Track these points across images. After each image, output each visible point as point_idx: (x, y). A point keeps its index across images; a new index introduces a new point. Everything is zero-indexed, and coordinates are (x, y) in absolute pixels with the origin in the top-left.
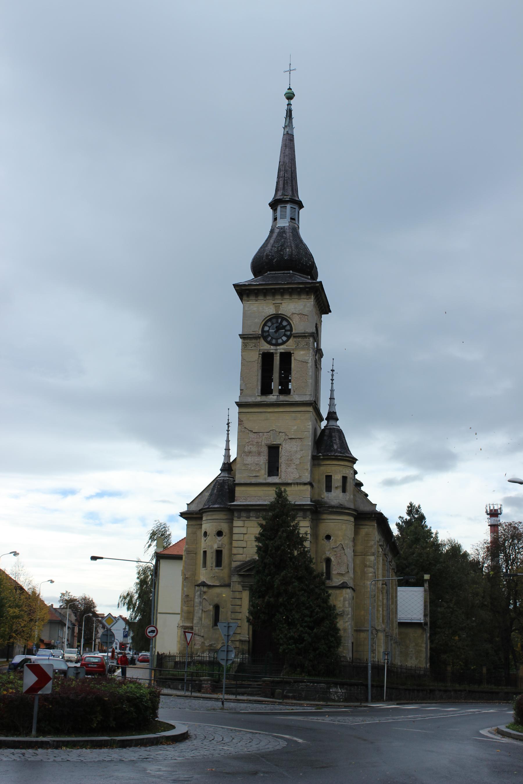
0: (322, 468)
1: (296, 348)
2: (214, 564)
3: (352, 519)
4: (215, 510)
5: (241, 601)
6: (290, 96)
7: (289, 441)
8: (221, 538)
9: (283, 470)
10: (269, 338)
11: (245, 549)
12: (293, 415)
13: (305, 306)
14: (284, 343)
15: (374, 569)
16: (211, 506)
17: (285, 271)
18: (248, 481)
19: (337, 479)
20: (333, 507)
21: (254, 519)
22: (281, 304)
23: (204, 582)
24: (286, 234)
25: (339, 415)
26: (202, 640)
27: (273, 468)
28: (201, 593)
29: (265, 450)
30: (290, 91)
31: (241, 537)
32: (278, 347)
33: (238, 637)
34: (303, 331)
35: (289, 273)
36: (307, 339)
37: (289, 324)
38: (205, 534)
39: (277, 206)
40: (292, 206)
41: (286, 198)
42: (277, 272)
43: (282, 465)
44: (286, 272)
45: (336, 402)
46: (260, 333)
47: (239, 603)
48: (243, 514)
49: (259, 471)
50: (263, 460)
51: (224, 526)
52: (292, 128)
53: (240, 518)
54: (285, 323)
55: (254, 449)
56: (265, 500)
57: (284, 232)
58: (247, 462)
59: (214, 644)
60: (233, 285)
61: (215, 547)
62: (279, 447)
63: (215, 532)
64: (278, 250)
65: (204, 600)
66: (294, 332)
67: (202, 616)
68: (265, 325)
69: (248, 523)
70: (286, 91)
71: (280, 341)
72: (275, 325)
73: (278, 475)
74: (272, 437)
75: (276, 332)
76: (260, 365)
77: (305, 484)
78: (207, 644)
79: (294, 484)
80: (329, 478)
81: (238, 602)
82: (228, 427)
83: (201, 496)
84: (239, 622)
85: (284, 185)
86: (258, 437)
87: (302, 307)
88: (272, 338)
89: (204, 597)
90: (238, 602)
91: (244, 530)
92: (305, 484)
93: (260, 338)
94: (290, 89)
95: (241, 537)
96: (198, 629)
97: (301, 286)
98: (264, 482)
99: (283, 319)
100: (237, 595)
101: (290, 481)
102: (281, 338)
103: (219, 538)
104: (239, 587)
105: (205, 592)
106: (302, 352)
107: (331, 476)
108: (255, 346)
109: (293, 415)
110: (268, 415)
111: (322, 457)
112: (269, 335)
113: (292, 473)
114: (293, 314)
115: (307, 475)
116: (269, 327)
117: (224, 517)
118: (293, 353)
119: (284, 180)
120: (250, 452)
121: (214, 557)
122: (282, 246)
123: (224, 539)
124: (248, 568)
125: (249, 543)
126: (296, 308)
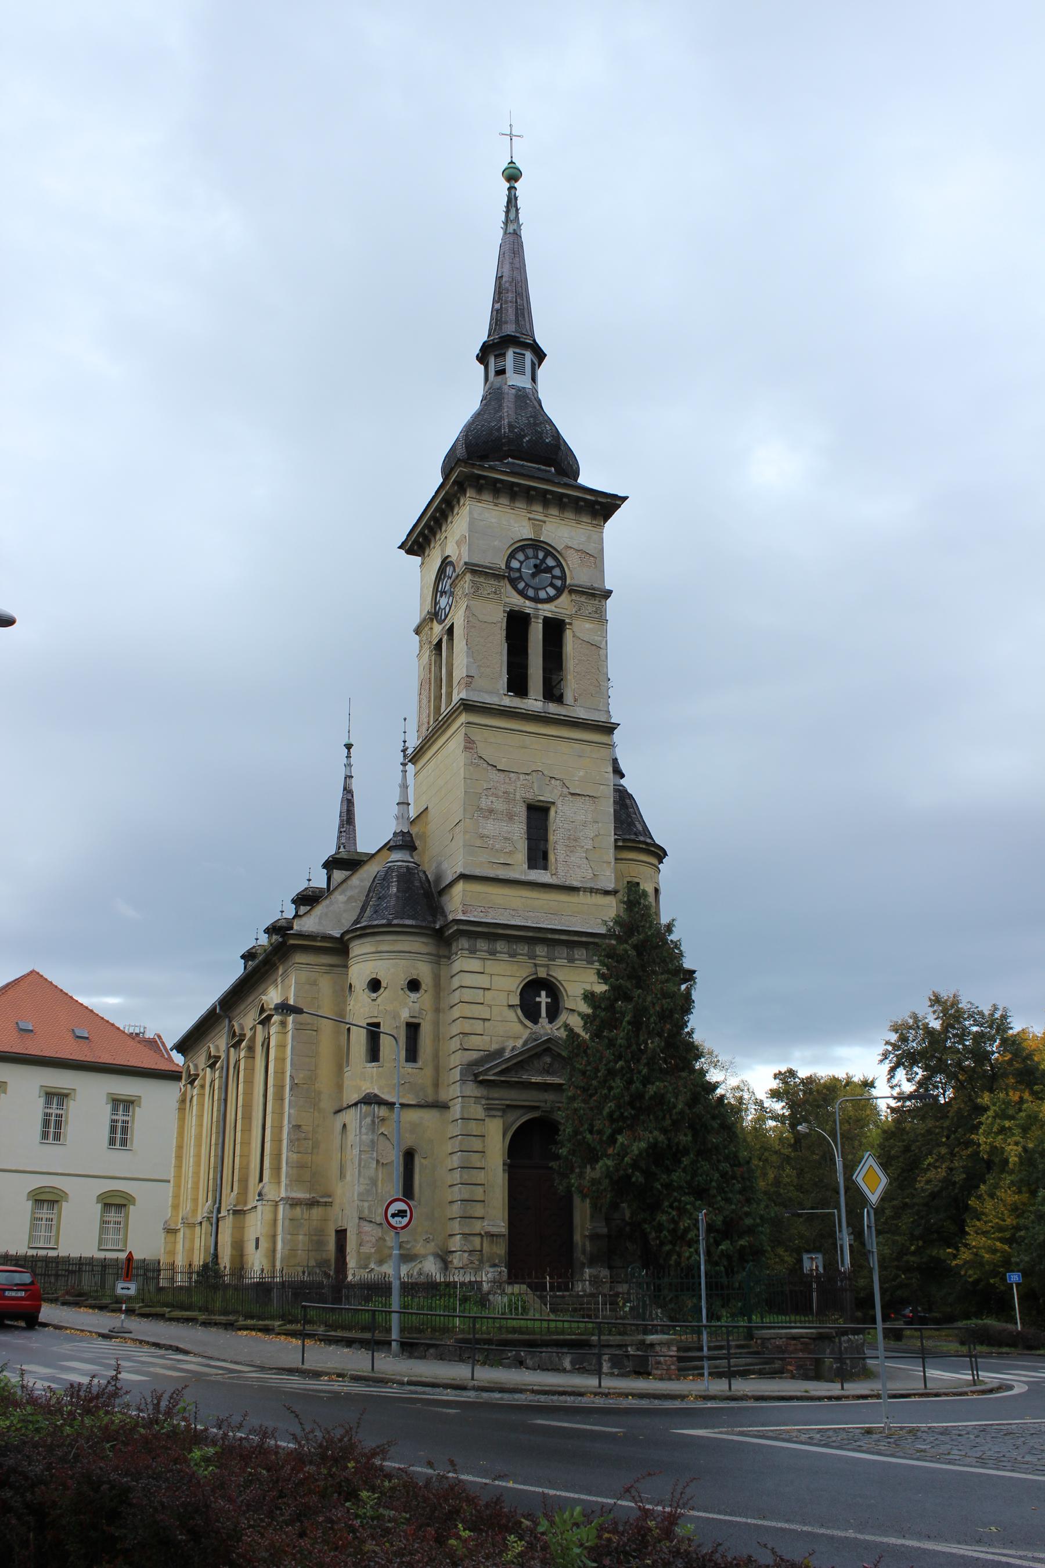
1: (577, 615)
2: (403, 1053)
4: (388, 930)
8: (418, 995)
9: (561, 857)
10: (521, 586)
11: (487, 1024)
14: (550, 600)
16: (395, 922)
18: (491, 873)
21: (505, 957)
22: (545, 522)
23: (376, 1095)
27: (538, 854)
28: (373, 1122)
29: (521, 811)
31: (479, 996)
32: (540, 606)
33: (478, 1227)
35: (550, 471)
36: (596, 602)
37: (559, 565)
38: (375, 985)
39: (508, 347)
40: (518, 351)
41: (510, 341)
44: (543, 467)
46: (503, 567)
48: (482, 945)
49: (510, 853)
50: (518, 830)
51: (423, 971)
53: (475, 953)
54: (550, 562)
55: (499, 805)
58: (486, 832)
59: (408, 1242)
61: (405, 1015)
63: (403, 983)
65: (381, 1138)
68: (512, 556)
69: (491, 966)
72: (532, 562)
74: (535, 786)
75: (534, 575)
76: (504, 633)
77: (607, 893)
79: (585, 890)
84: (480, 1189)
86: (507, 781)
87: (583, 539)
88: (527, 585)
91: (483, 981)
92: (607, 893)
95: (479, 996)
96: (369, 1207)
97: (589, 497)
98: (523, 878)
99: (548, 554)
100: (474, 1128)
101: (576, 884)
102: (544, 588)
103: (414, 996)
104: (478, 1111)
105: (383, 1120)
106: (588, 625)
107: (638, 884)
108: (495, 593)
110: (528, 740)
112: (521, 578)
113: (579, 867)
115: (608, 874)
116: (521, 563)
117: (424, 949)
118: (570, 624)
120: (491, 811)
123: (422, 1000)
124: (504, 1067)
126: (561, 531)
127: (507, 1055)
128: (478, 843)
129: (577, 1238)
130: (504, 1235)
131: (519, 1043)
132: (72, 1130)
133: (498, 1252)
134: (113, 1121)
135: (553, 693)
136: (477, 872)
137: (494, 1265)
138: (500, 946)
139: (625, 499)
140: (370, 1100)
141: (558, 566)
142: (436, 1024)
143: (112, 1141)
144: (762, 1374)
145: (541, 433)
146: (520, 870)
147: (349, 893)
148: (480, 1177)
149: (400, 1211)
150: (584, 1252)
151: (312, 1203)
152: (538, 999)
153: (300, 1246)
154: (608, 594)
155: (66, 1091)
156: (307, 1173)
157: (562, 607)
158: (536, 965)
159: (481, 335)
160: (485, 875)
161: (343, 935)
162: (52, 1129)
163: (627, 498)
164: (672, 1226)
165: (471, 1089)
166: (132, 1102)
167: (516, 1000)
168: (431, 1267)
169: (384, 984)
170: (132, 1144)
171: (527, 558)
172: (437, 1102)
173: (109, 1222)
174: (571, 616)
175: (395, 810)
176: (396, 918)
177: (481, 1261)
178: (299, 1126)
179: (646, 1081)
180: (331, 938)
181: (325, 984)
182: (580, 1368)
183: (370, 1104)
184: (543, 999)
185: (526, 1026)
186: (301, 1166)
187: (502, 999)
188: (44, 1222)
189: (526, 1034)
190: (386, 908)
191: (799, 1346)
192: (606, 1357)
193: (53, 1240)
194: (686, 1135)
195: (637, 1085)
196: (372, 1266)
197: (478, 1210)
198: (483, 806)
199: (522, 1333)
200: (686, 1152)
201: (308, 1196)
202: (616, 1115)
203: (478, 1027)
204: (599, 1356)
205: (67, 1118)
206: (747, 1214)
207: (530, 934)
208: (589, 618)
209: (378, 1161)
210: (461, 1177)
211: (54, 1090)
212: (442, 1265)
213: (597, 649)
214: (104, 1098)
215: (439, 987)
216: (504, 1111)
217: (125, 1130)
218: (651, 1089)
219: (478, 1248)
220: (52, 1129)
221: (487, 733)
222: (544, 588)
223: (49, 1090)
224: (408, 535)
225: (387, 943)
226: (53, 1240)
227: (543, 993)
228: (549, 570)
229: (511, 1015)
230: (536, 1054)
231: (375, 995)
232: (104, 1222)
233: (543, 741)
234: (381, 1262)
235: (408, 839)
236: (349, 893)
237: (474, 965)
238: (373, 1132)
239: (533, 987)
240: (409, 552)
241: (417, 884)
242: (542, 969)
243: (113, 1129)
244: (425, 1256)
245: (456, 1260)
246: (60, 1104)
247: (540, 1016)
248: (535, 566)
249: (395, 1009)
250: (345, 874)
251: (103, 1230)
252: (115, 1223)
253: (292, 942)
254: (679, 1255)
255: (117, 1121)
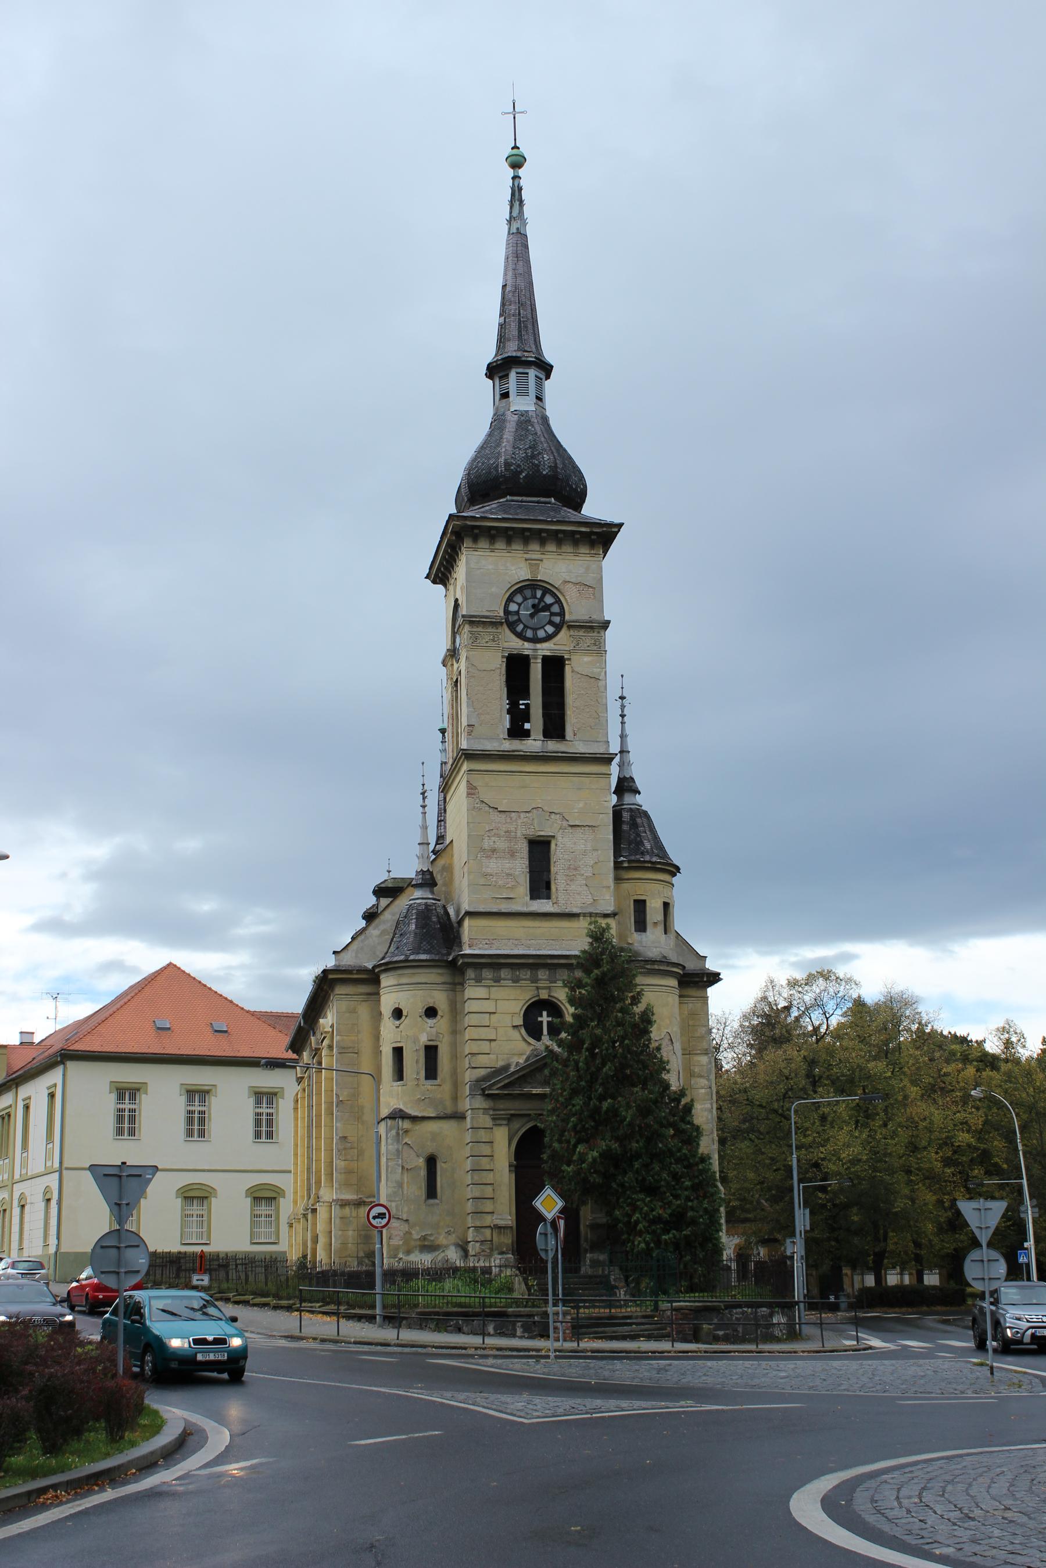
0: (626, 886)
3: (674, 983)
4: (406, 965)
5: (492, 1147)
6: (516, 163)
7: (570, 830)
8: (434, 1021)
10: (520, 628)
11: (493, 1043)
12: (576, 779)
13: (588, 568)
14: (549, 638)
15: (709, 1080)
16: (412, 957)
17: (523, 496)
19: (654, 907)
20: (654, 962)
21: (509, 983)
22: (541, 560)
23: (401, 1110)
24: (533, 426)
25: (639, 784)
26: (405, 1227)
27: (540, 883)
28: (398, 1134)
29: (523, 848)
30: (515, 151)
31: (485, 1019)
32: (539, 646)
33: (488, 1220)
34: (587, 618)
36: (595, 634)
37: (558, 601)
38: (398, 1014)
39: (510, 368)
40: (520, 370)
41: (517, 360)
42: (525, 499)
43: (558, 877)
44: (543, 499)
45: (632, 757)
46: (502, 614)
47: (488, 1152)
48: (487, 973)
49: (512, 888)
50: (520, 866)
51: (440, 999)
52: (524, 223)
53: (480, 982)
54: (549, 600)
55: (501, 844)
56: (529, 947)
57: (528, 421)
58: (489, 871)
60: (622, 524)
61: (424, 1039)
62: (548, 843)
64: (527, 456)
65: (405, 1147)
66: (567, 617)
67: (402, 1179)
68: (510, 600)
69: (497, 992)
70: (508, 151)
71: (541, 634)
72: (530, 602)
73: (548, 897)
74: (536, 821)
75: (532, 616)
76: (504, 678)
78: (416, 1236)
80: (640, 906)
81: (486, 1150)
82: (424, 798)
83: (362, 937)
84: (490, 1188)
85: (520, 331)
88: (525, 626)
89: (406, 1140)
90: (486, 1150)
91: (489, 1006)
93: (501, 624)
94: (515, 147)
95: (485, 1019)
96: (397, 1206)
97: (583, 529)
98: (525, 909)
99: (546, 591)
100: (483, 1135)
101: (575, 910)
102: (543, 627)
103: (431, 1022)
104: (486, 1121)
105: (406, 1131)
106: (586, 659)
107: (644, 901)
108: (493, 640)
109: (576, 779)
110: (527, 779)
111: (626, 865)
112: (519, 620)
114: (566, 582)
116: (519, 605)
117: (440, 979)
118: (569, 659)
119: (520, 322)
120: (494, 851)
121: (422, 1060)
122: (533, 447)
123: (441, 1024)
124: (506, 1081)
125: (501, 1031)
126: (558, 567)
127: (512, 1069)
128: (482, 881)
129: (582, 1227)
130: (511, 1227)
131: (521, 1061)
132: (216, 1124)
133: (506, 1241)
134: (257, 1114)
135: (555, 728)
136: (481, 909)
137: (502, 1253)
138: (504, 973)
139: (621, 525)
140: (398, 1115)
141: (556, 602)
142: (454, 1045)
143: (258, 1135)
144: (649, 1337)
145: (538, 466)
146: (523, 902)
147: (382, 927)
148: (489, 1177)
149: (380, 1214)
150: (586, 1240)
151: (359, 1204)
152: (540, 1019)
153: (350, 1240)
154: (606, 625)
155: (206, 1088)
156: (354, 1178)
157: (560, 644)
158: (538, 988)
159: (489, 353)
160: (488, 910)
161: (374, 967)
162: (126, 1124)
163: (622, 524)
164: (626, 1219)
165: (480, 1102)
166: (275, 1094)
167: (519, 1021)
168: (453, 1255)
169: (405, 1013)
170: (278, 1135)
171: (525, 599)
172: (456, 1113)
173: (260, 1216)
174: (570, 652)
175: (417, 850)
176: (413, 953)
177: (491, 1249)
178: (345, 1137)
179: (602, 1098)
180: (365, 971)
181: (364, 1011)
182: (500, 1333)
183: (394, 1118)
184: (545, 1018)
185: (529, 1044)
186: (348, 1172)
187: (508, 1021)
188: (195, 1218)
189: (528, 1050)
190: (405, 944)
191: (680, 1316)
192: (519, 1324)
193: (205, 1236)
194: (637, 1142)
195: (594, 1102)
196: (401, 1255)
197: (488, 1206)
198: (486, 846)
199: (462, 1307)
200: (637, 1156)
201: (354, 1197)
202: (579, 1128)
203: (485, 1047)
204: (514, 1324)
205: (210, 1114)
206: (692, 1209)
207: (531, 961)
208: (588, 651)
209: (403, 1167)
210: (472, 1178)
211: (194, 1088)
212: (462, 1253)
213: (596, 680)
214: (246, 1092)
215: (456, 1011)
216: (509, 1120)
217: (270, 1123)
218: (605, 1105)
219: (489, 1238)
220: (126, 1124)
221: (487, 778)
222: (543, 627)
223: (190, 1088)
224: (431, 568)
225: (407, 977)
226: (205, 1236)
227: (545, 1013)
228: (547, 607)
229: (515, 1034)
230: (537, 1068)
231: (398, 1022)
232: (255, 1216)
233: (543, 779)
234: (408, 1252)
235: (428, 877)
236: (382, 927)
237: (480, 992)
238: (398, 1141)
239: (534, 1009)
240: (434, 582)
241: (434, 919)
242: (544, 991)
243: (258, 1123)
244: (447, 1247)
245: (473, 1248)
246: (203, 1101)
247: (541, 1033)
248: (534, 606)
249: (416, 1033)
250: (388, 900)
251: (254, 1224)
252: (266, 1216)
253: (330, 976)
254: (633, 1243)
255: (261, 1114)
